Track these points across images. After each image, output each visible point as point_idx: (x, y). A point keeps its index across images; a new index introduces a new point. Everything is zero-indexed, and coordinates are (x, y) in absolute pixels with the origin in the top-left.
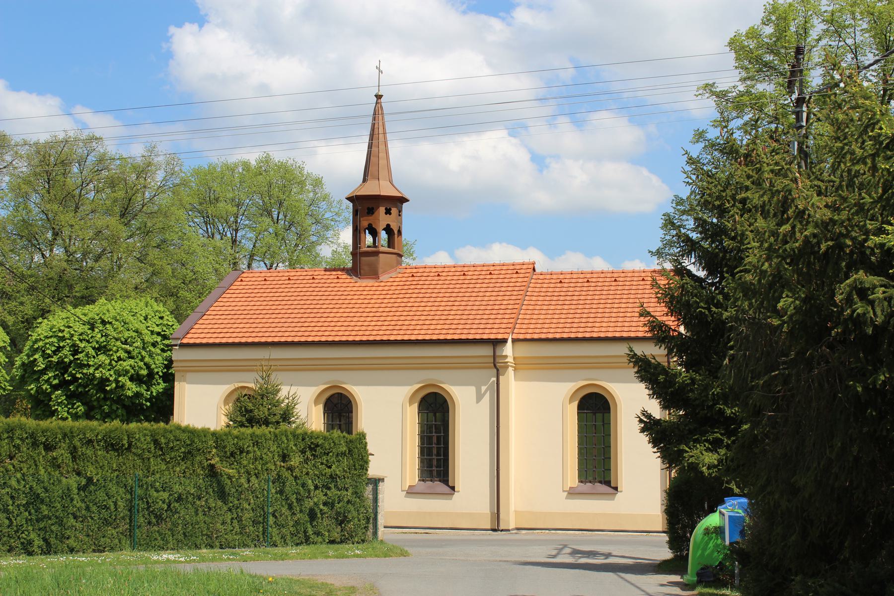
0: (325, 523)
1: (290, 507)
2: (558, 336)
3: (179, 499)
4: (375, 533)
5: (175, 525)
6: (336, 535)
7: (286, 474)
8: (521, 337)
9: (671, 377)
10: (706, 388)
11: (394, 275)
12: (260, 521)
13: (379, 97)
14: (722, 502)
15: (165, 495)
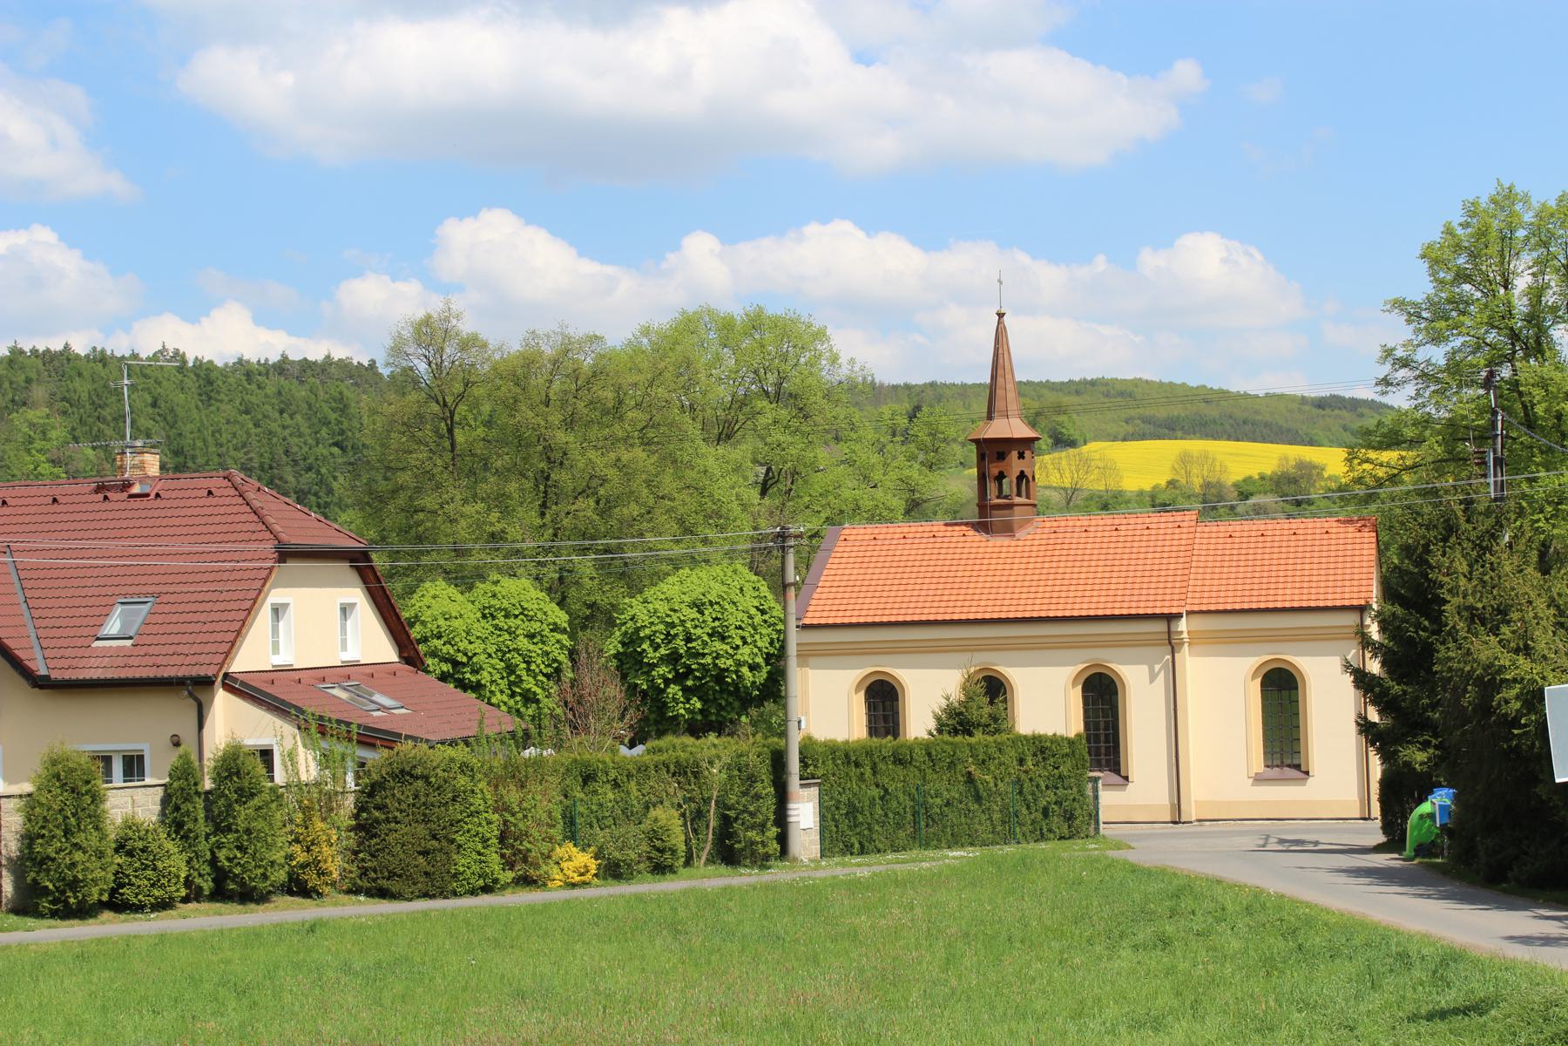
0: (1056, 821)
1: (1028, 808)
2: (1237, 607)
3: (948, 804)
4: (1097, 829)
5: (945, 827)
6: (1066, 832)
7: (1023, 776)
8: (1196, 608)
9: (1385, 691)
10: (1417, 699)
11: (1030, 529)
12: (1009, 817)
13: (1001, 315)
14: (1431, 793)
15: (938, 801)
